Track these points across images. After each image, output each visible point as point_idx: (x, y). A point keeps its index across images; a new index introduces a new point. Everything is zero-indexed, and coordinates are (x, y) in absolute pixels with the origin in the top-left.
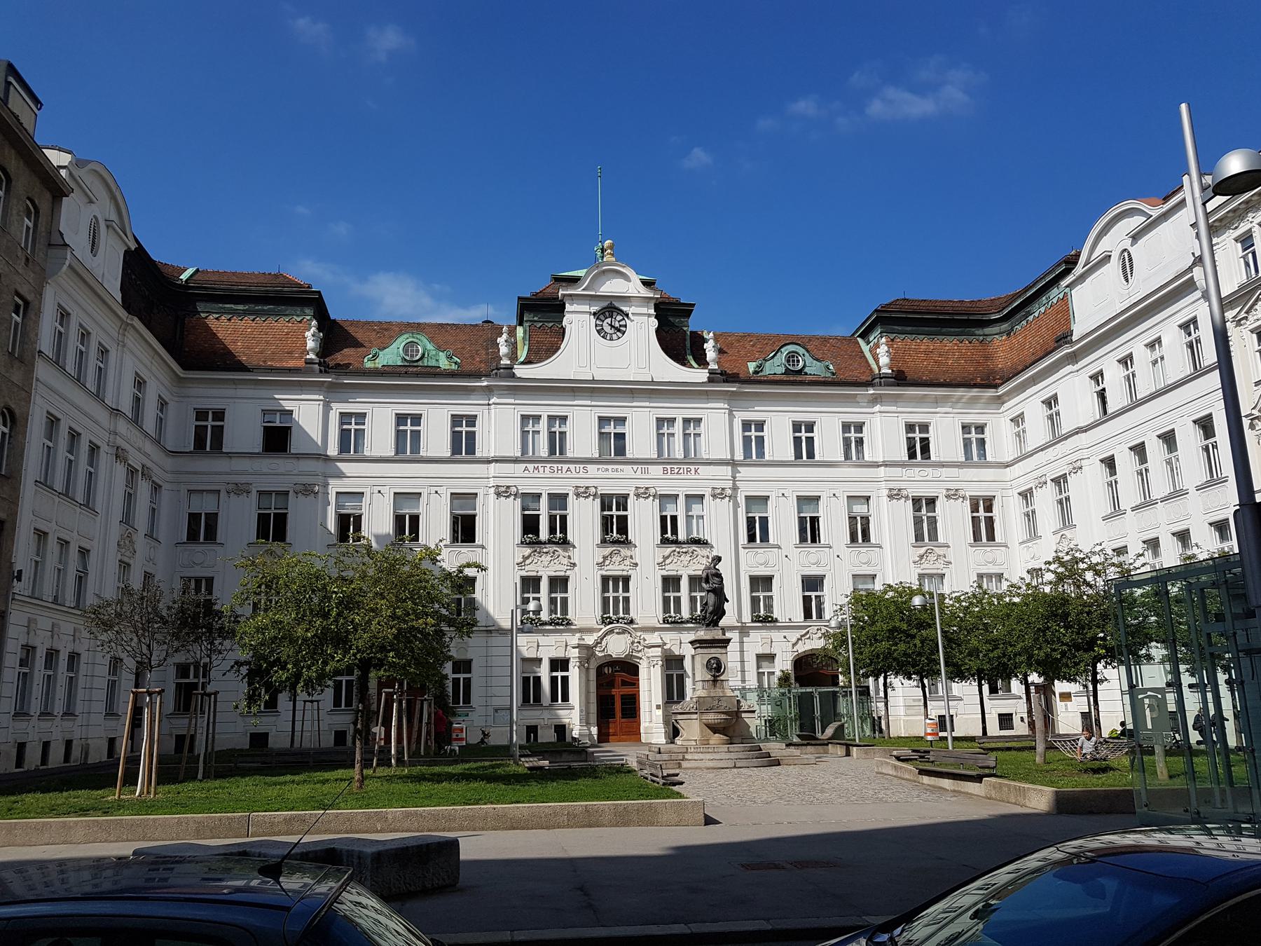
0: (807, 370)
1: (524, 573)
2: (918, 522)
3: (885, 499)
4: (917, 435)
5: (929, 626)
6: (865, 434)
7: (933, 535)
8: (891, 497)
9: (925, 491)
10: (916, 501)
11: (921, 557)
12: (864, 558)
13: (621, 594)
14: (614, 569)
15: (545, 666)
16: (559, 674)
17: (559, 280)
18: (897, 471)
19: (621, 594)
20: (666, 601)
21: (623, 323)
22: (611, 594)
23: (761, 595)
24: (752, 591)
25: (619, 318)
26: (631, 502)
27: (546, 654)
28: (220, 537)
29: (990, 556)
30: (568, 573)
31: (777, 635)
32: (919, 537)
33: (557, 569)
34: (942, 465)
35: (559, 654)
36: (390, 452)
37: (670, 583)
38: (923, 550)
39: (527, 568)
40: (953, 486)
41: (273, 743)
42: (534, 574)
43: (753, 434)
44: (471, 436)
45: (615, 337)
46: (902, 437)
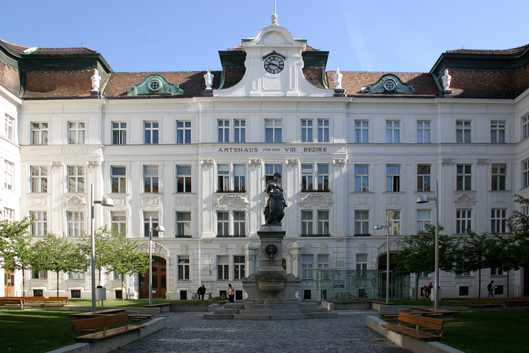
0: (398, 90)
1: (303, 209)
2: (459, 179)
3: (440, 166)
4: (152, 129)
5: (431, 239)
6: (330, 127)
7: (468, 188)
8: (443, 164)
9: (464, 161)
10: (459, 167)
11: (459, 199)
12: (362, 200)
13: (466, 219)
14: (464, 206)
15: (231, 260)
16: (239, 264)
17: (244, 41)
18: (448, 149)
19: (466, 219)
20: (304, 224)
21: (282, 63)
22: (496, 218)
23: (362, 221)
24: (356, 218)
25: (279, 60)
26: (85, 171)
27: (232, 253)
28: (473, 188)
29: (38, 201)
30: (328, 208)
31: (331, 244)
32: (459, 188)
33: (322, 207)
34: (477, 144)
35: (239, 253)
36: (216, 141)
37: (307, 214)
38: (461, 195)
39: (305, 205)
40: (482, 157)
41: (46, 296)
42: (309, 209)
43: (240, 127)
44: (188, 132)
45: (276, 71)
46: (454, 127)
